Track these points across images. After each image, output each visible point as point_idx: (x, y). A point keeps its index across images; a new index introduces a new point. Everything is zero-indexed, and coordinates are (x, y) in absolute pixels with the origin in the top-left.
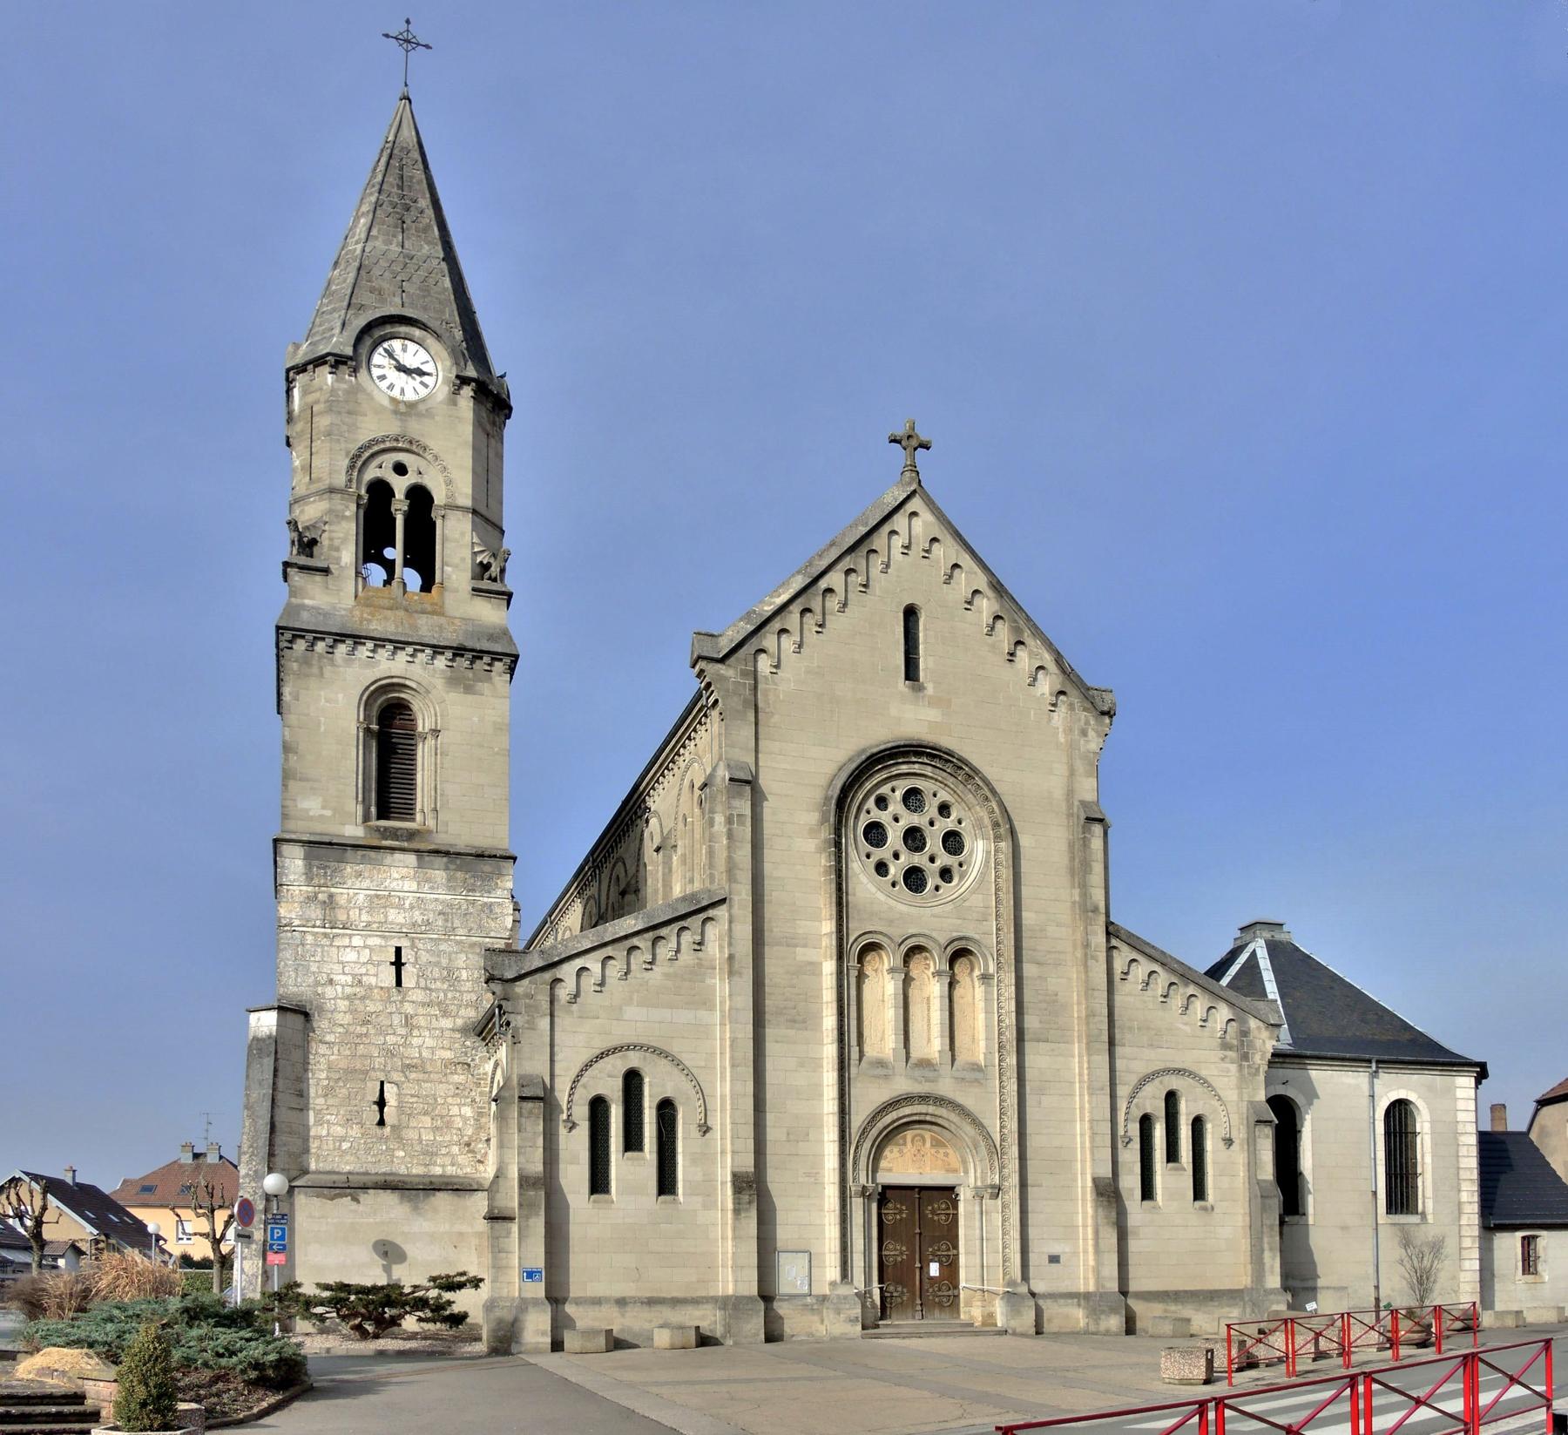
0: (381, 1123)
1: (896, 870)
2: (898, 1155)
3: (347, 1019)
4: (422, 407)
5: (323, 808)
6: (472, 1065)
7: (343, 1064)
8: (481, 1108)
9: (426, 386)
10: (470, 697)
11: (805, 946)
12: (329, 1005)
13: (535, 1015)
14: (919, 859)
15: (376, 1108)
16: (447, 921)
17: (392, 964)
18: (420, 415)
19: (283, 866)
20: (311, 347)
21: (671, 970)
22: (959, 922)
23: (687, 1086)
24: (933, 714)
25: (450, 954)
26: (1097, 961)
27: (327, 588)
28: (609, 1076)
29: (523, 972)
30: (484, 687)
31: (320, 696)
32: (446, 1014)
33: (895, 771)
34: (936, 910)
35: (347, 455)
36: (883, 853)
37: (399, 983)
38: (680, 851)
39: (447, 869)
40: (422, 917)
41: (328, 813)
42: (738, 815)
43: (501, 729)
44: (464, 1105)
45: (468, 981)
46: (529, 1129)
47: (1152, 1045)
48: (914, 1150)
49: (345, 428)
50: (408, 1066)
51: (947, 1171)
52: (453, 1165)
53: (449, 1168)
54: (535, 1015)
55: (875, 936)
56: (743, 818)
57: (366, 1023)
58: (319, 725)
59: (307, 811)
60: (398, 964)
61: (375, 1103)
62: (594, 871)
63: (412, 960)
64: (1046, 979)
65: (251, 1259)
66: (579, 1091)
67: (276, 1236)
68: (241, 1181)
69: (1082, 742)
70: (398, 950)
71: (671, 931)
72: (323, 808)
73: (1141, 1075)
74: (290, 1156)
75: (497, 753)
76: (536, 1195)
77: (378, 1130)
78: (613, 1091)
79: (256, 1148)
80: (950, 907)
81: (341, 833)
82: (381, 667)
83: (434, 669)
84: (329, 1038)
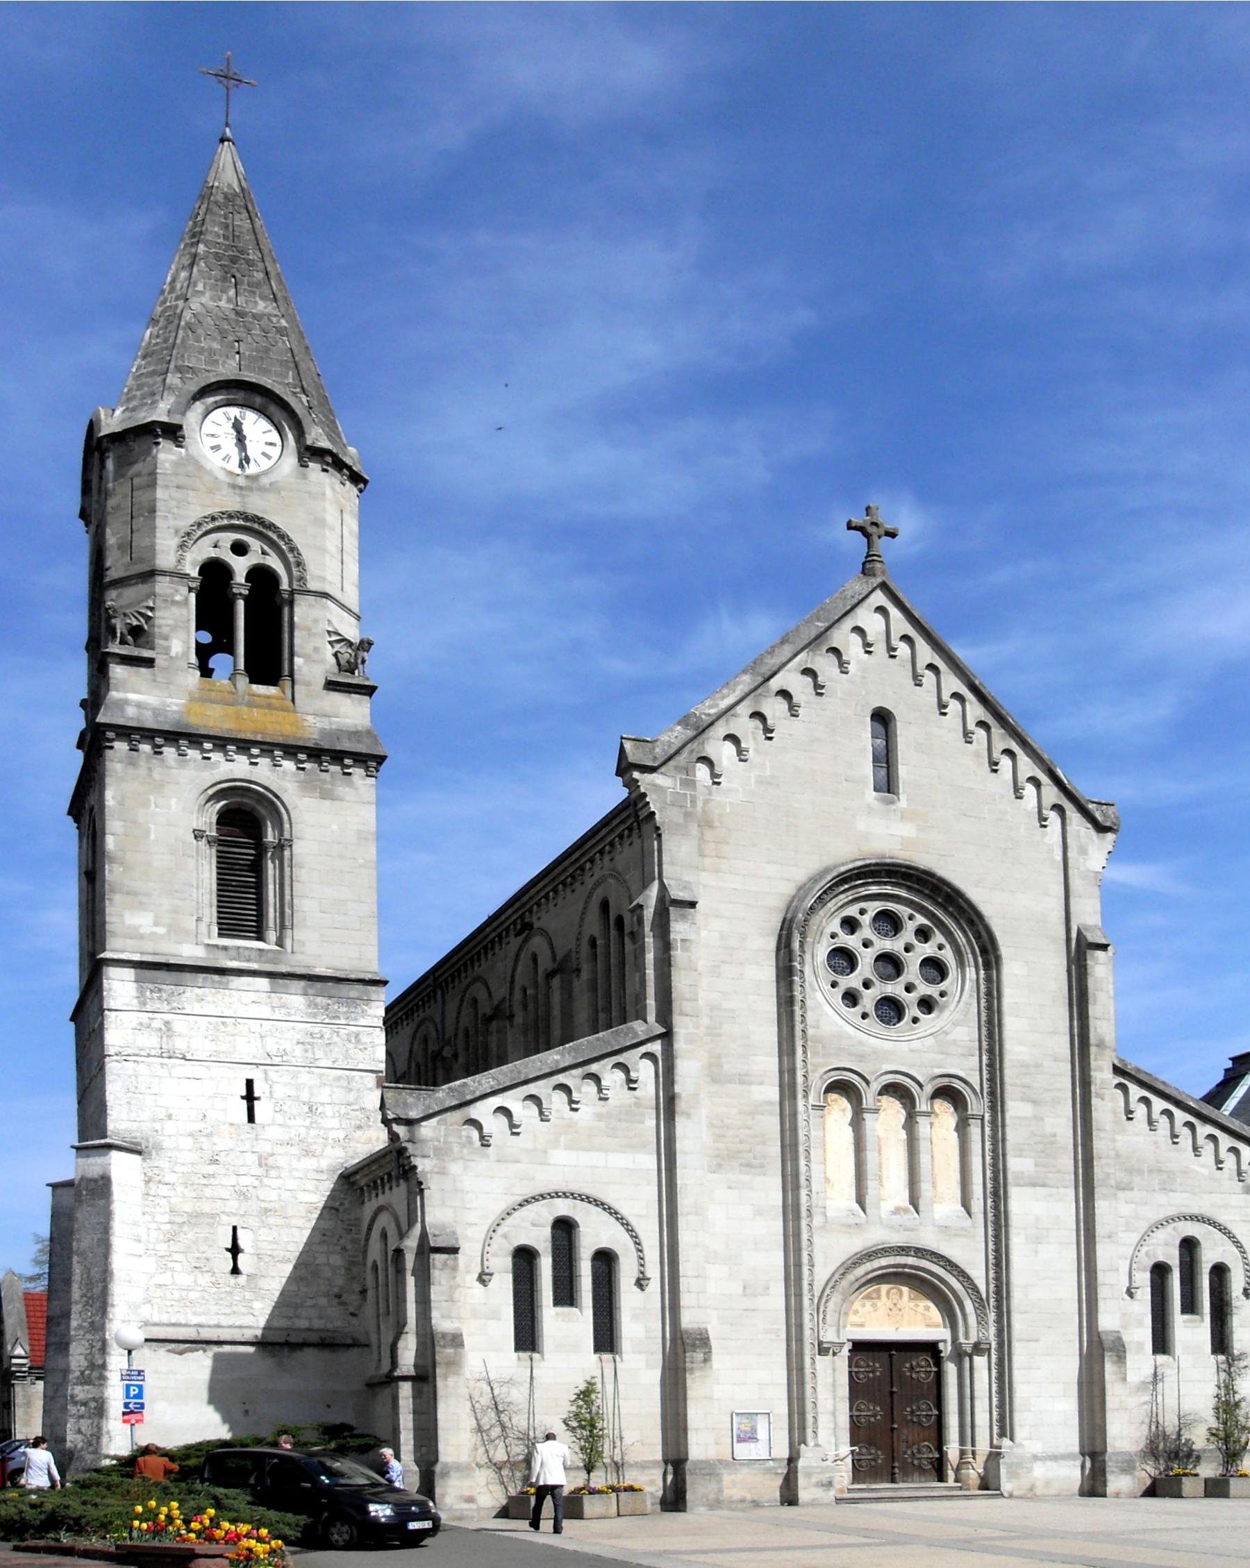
0: (235, 1271)
1: (869, 999)
2: (871, 1309)
3: (193, 1157)
4: (265, 481)
5: (156, 924)
6: (341, 1209)
7: (188, 1208)
8: (353, 1256)
9: (269, 457)
10: (327, 803)
11: (761, 1083)
12: (167, 1143)
13: (446, 1159)
14: (895, 989)
15: (229, 1255)
16: (306, 1051)
17: (243, 1098)
18: (262, 489)
19: (110, 989)
20: (128, 414)
21: (604, 1110)
22: (941, 1056)
23: (625, 1237)
24: (907, 830)
25: (311, 1088)
26: (1103, 1099)
27: (154, 681)
28: (534, 1225)
29: (431, 1111)
30: (342, 790)
31: (149, 800)
32: (308, 1153)
33: (864, 891)
34: (916, 1045)
35: (177, 532)
36: (853, 981)
37: (251, 1119)
38: (585, 975)
39: (305, 994)
40: (277, 1046)
41: (161, 930)
42: (683, 940)
43: (366, 839)
44: (333, 1253)
45: (334, 1117)
46: (443, 1282)
47: (1164, 1189)
48: (889, 1304)
49: (174, 503)
50: (266, 1210)
51: (928, 1326)
52: (320, 1318)
53: (317, 1321)
54: (446, 1159)
55: (967, 1088)
56: (688, 944)
57: (215, 1162)
58: (148, 833)
59: (136, 928)
60: (250, 1097)
61: (228, 1250)
62: (435, 992)
63: (268, 1094)
64: (1042, 1119)
65: (90, 1418)
66: (498, 1242)
67: (132, 1393)
68: (72, 1333)
69: (1082, 860)
70: (250, 1084)
71: (605, 1065)
72: (156, 924)
73: (1152, 1221)
74: (130, 1307)
75: (360, 866)
76: (455, 1353)
77: (232, 1280)
78: (541, 1240)
79: (90, 1298)
80: (930, 1041)
81: (178, 953)
82: (222, 769)
83: (284, 772)
84: (170, 1178)
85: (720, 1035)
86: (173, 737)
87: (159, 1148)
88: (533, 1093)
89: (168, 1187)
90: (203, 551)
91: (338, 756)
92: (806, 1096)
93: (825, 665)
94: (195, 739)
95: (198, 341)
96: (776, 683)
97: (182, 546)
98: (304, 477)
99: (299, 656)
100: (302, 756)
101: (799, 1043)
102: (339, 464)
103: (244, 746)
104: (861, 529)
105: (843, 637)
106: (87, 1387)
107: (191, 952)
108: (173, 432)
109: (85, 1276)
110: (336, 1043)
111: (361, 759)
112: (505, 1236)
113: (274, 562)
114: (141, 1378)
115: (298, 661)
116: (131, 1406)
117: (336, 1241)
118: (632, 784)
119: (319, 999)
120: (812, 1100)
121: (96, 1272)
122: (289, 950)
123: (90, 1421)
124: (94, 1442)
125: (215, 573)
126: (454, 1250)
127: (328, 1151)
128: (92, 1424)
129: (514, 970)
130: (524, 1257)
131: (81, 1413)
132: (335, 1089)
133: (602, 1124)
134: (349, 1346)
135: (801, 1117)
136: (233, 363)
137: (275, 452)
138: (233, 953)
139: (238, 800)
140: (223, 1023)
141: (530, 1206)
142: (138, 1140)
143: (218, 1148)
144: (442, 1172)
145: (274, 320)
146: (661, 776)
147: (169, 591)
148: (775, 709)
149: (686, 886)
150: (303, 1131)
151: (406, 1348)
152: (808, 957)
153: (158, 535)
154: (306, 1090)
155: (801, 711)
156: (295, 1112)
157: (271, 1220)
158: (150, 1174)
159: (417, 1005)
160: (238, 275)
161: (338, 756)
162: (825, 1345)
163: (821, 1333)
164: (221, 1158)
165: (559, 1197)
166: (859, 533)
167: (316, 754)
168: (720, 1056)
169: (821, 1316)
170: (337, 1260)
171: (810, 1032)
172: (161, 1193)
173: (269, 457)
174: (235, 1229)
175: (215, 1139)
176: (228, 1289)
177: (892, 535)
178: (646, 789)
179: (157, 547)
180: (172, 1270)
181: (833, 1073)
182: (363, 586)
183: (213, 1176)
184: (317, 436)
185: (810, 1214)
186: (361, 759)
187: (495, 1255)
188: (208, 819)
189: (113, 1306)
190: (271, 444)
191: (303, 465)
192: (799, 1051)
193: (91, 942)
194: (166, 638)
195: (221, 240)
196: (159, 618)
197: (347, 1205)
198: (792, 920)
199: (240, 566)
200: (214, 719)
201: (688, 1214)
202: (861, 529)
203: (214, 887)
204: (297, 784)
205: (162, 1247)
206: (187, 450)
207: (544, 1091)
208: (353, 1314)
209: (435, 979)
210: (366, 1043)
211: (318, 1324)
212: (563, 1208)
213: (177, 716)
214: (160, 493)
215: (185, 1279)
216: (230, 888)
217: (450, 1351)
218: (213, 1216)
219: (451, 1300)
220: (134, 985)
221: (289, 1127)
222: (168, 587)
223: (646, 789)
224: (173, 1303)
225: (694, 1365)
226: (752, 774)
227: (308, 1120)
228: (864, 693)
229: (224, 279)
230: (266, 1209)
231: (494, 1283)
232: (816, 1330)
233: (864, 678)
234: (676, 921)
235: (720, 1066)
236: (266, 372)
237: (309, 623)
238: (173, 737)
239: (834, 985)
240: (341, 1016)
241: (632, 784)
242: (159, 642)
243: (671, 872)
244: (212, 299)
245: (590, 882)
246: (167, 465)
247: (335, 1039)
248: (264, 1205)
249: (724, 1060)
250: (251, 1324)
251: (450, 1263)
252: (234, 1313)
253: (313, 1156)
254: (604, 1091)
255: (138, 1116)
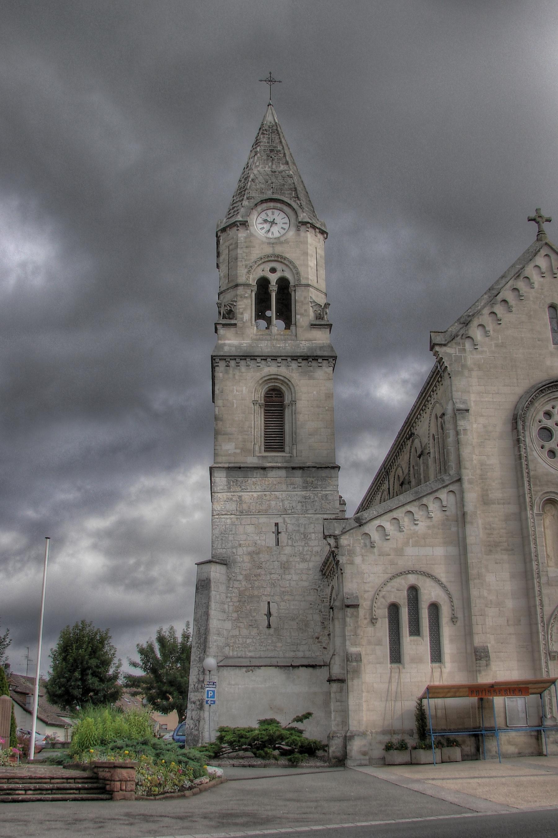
0: (269, 626)
6: (319, 589)
9: (284, 229)
12: (239, 559)
15: (266, 617)
16: (303, 506)
19: (215, 482)
25: (305, 525)
27: (237, 333)
28: (398, 590)
32: (304, 560)
40: (289, 505)
57: (260, 567)
63: (285, 530)
67: (210, 695)
70: (277, 525)
78: (402, 598)
85: (486, 479)
86: (244, 357)
87: (235, 562)
88: (395, 517)
89: (238, 582)
90: (258, 273)
91: (315, 358)
92: (532, 509)
93: (521, 284)
94: (253, 357)
95: (256, 185)
96: (499, 298)
97: (249, 272)
98: (299, 235)
99: (298, 315)
100: (300, 360)
101: (526, 479)
102: (314, 227)
103: (274, 358)
104: (534, 220)
105: (530, 271)
106: (196, 693)
107: (251, 461)
108: (244, 224)
109: (198, 632)
110: (316, 501)
111: (325, 358)
112: (383, 597)
113: (288, 275)
114: (215, 686)
115: (298, 317)
116: (209, 702)
117: (316, 607)
118: (436, 354)
119: (308, 479)
120: (535, 511)
121: (203, 630)
122: (295, 455)
123: (196, 712)
124: (197, 724)
125: (263, 283)
126: (356, 606)
127: (313, 558)
128: (197, 714)
129: (410, 458)
130: (394, 609)
131: (193, 708)
132: (316, 525)
133: (430, 532)
134: (320, 666)
135: (530, 521)
136: (270, 192)
137: (286, 226)
138: (269, 459)
139: (273, 384)
140: (265, 495)
141: (395, 580)
142: (225, 558)
143: (262, 560)
144: (352, 563)
145: (287, 172)
146: (449, 348)
147: (243, 293)
148: (499, 309)
149: (464, 402)
150: (301, 548)
151: (335, 664)
152: (527, 433)
153: (238, 269)
154: (303, 526)
155: (514, 309)
156: (297, 538)
157: (286, 598)
158: (230, 576)
159: (380, 483)
160: (273, 157)
161: (315, 358)
162: (553, 654)
163: (550, 647)
164: (264, 565)
165: (410, 573)
166: (534, 222)
167: (306, 358)
168: (487, 490)
169: (549, 637)
170: (317, 618)
171: (532, 473)
172: (235, 586)
173: (284, 229)
174: (269, 603)
175: (261, 555)
176: (265, 637)
177: (549, 220)
178: (442, 355)
179: (238, 274)
180: (239, 627)
181: (546, 495)
182: (327, 280)
183: (259, 575)
184: (304, 216)
185: (539, 577)
186: (325, 358)
187: (378, 608)
188: (260, 395)
189: (209, 648)
190: (285, 223)
191: (299, 230)
192: (526, 484)
193: (226, 465)
194: (242, 314)
195: (267, 144)
196: (239, 305)
197: (322, 587)
198: (517, 415)
199: (273, 278)
200: (265, 347)
201: (475, 579)
202: (534, 220)
203: (263, 428)
204: (298, 374)
205: (235, 615)
206: (250, 231)
207: (400, 515)
208: (324, 648)
209: (385, 469)
210: (330, 500)
211: (308, 654)
212: (412, 579)
213: (245, 348)
214: (239, 251)
215: (245, 632)
216: (271, 427)
217: (355, 664)
218: (259, 597)
219: (356, 634)
220: (226, 479)
221: (294, 546)
222: (243, 291)
223: (442, 355)
224: (239, 645)
225: (481, 668)
226: (493, 343)
227: (304, 542)
228: (543, 297)
229: (268, 160)
230: (283, 592)
231: (378, 625)
232: (546, 644)
233: (542, 289)
234: (460, 420)
235: (488, 495)
236: (283, 194)
237: (302, 299)
238: (244, 357)
239: (542, 447)
240: (319, 487)
241: (436, 354)
242: (239, 316)
243: (457, 395)
244: (262, 168)
245: (430, 406)
246: (242, 238)
247: (316, 499)
248: (283, 589)
249: (489, 492)
250: (276, 656)
251: (355, 613)
252: (268, 650)
253: (306, 561)
254: (430, 514)
255: (226, 546)
